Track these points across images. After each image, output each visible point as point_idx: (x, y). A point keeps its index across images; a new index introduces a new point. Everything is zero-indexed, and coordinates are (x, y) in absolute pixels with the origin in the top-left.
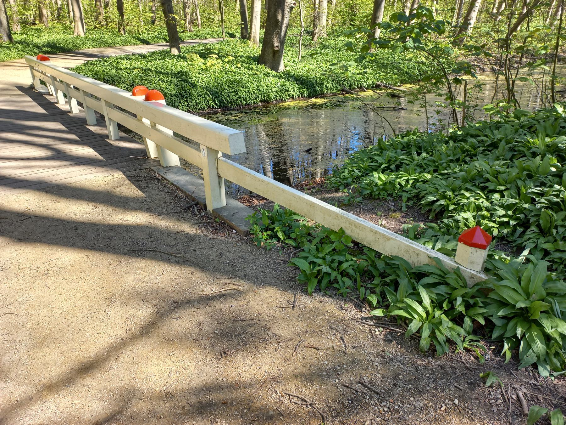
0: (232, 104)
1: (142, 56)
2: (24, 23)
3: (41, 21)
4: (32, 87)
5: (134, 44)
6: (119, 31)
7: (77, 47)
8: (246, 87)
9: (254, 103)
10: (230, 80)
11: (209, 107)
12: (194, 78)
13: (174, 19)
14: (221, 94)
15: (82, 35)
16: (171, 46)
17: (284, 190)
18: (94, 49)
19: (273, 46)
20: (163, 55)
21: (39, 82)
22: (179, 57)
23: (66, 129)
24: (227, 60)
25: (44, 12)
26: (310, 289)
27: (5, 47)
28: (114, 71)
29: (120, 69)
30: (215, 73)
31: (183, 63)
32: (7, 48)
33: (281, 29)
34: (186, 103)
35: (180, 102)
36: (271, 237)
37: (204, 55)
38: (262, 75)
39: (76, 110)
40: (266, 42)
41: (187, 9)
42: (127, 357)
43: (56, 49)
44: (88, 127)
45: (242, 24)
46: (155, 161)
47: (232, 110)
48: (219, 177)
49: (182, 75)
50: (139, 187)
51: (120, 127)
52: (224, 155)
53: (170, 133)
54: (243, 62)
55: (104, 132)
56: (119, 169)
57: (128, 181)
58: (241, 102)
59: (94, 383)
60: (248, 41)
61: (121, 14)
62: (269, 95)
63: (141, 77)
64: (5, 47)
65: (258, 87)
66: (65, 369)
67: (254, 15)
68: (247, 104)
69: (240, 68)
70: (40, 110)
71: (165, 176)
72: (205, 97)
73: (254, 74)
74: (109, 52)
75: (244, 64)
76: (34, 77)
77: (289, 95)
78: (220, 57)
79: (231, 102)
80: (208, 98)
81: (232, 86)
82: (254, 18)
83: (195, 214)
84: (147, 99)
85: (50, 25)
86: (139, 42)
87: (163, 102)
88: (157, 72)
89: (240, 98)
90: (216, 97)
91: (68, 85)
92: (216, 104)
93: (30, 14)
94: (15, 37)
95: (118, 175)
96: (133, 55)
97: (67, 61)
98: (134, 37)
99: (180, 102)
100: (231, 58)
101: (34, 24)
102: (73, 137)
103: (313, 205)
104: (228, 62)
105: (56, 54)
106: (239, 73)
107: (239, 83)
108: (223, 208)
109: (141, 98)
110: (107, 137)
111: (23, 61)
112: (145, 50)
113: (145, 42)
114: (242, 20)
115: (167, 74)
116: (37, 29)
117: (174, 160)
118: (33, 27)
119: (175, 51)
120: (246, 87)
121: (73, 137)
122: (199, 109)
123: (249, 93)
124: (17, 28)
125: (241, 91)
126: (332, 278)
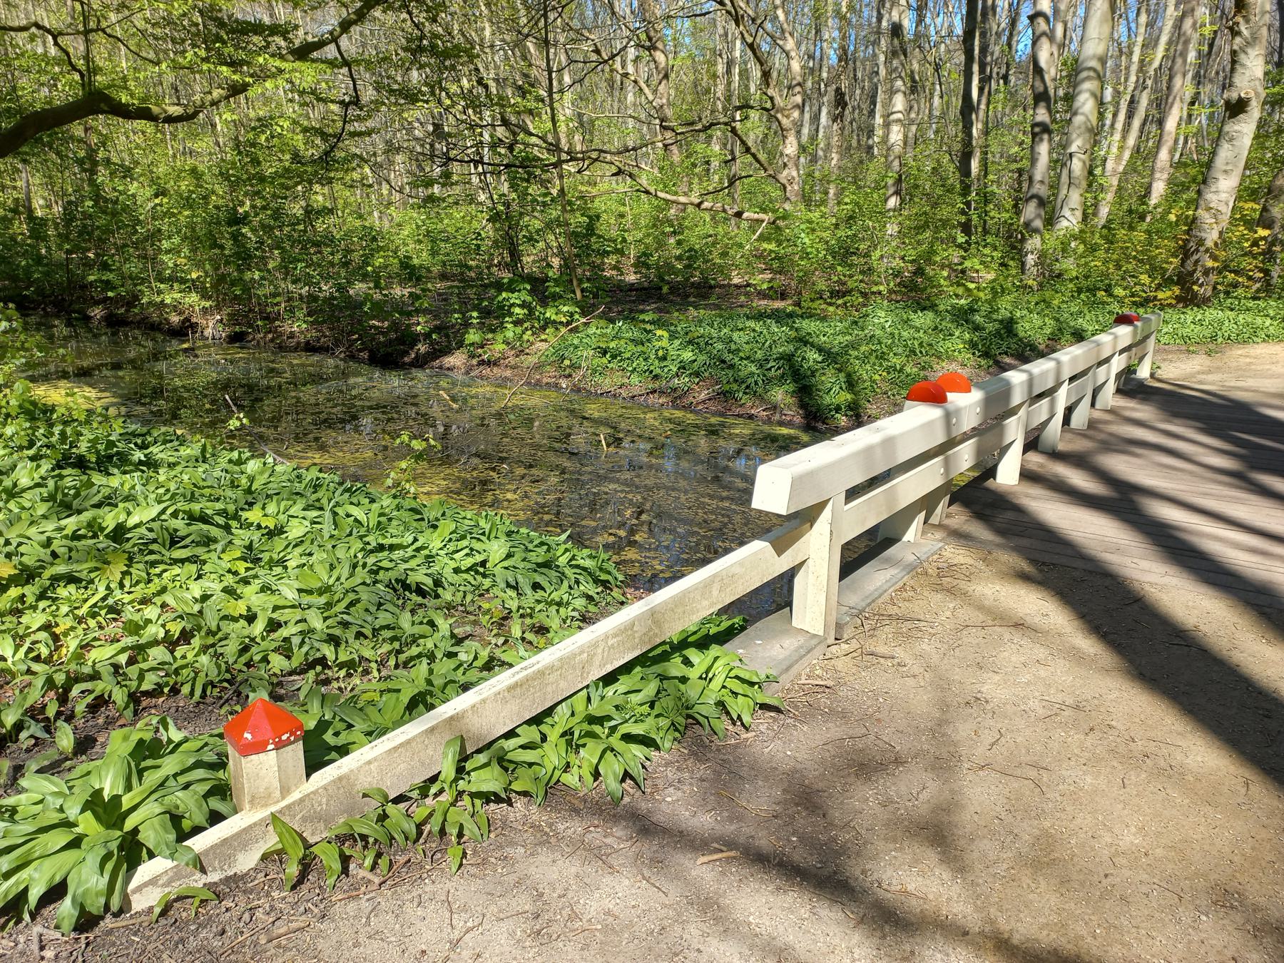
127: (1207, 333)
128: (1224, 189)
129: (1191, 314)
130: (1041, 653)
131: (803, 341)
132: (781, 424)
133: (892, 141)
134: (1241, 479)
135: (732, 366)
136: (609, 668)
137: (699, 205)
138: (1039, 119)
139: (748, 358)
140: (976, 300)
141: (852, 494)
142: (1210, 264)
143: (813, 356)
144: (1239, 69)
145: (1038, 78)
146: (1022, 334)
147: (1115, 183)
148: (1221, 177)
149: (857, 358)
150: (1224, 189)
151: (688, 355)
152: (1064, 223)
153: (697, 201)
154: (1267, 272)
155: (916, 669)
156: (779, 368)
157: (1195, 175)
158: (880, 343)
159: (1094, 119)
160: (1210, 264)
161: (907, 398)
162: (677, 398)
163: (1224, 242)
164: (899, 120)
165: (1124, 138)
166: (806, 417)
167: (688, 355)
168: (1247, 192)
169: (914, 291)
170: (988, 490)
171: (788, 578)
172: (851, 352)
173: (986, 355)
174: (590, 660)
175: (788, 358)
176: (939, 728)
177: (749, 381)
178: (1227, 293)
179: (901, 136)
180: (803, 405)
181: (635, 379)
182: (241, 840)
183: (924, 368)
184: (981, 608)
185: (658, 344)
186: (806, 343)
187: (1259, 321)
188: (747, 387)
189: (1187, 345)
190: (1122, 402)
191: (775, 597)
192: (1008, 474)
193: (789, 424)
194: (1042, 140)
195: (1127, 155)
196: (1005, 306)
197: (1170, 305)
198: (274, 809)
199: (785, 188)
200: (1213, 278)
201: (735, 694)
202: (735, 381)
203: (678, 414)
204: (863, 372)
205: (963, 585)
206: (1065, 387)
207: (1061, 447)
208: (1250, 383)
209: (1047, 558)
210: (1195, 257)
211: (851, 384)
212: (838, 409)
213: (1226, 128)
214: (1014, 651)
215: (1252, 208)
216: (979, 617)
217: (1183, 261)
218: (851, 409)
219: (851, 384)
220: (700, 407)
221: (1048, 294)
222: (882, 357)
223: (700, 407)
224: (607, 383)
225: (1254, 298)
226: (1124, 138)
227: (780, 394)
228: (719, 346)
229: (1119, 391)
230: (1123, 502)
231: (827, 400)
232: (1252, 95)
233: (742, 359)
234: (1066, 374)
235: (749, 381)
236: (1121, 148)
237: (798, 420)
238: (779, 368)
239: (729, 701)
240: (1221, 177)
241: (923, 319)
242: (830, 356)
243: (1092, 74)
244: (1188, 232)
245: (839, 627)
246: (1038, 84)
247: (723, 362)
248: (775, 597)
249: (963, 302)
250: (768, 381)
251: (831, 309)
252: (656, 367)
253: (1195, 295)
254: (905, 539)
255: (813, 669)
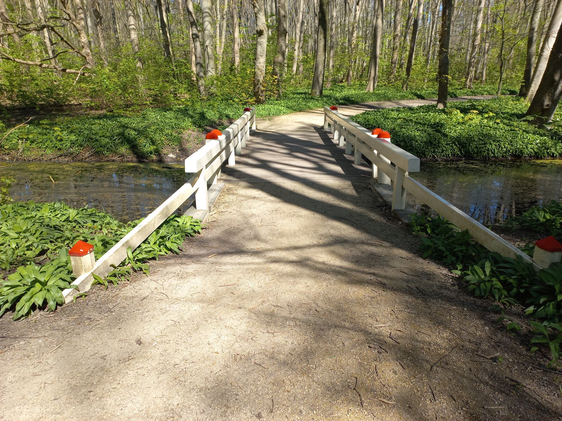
0: (478, 155)
1: (411, 109)
2: (335, 81)
3: (347, 80)
4: (322, 128)
5: (410, 99)
6: (402, 88)
7: (363, 100)
8: (498, 141)
9: (503, 156)
10: (483, 134)
11: (454, 155)
12: (448, 130)
13: (447, 79)
14: (469, 145)
15: (371, 91)
16: (439, 101)
17: (437, 200)
18: (376, 102)
19: (542, 105)
20: (428, 109)
21: (327, 125)
22: (443, 111)
23: (343, 172)
24: (486, 115)
25: (351, 73)
26: (425, 255)
27: (316, 99)
28: (382, 120)
29: (388, 118)
30: (470, 126)
31: (444, 116)
32: (317, 100)
33: (555, 90)
34: (432, 150)
35: (428, 148)
36: (422, 230)
37: (465, 111)
38: (521, 131)
39: (342, 143)
40: (537, 101)
41: (471, 68)
42: (313, 250)
43: (348, 102)
44: (354, 165)
45: (523, 82)
46: (375, 179)
47: (476, 160)
48: (403, 188)
49: (438, 126)
50: (357, 192)
51: (363, 157)
52: (410, 174)
53: (389, 162)
54: (504, 118)
55: (352, 158)
56: (351, 180)
57: (352, 187)
58: (488, 154)
59: (298, 252)
60: (522, 99)
61: (408, 74)
62: (521, 151)
63: (402, 125)
64: (316, 99)
65: (511, 142)
66: (288, 246)
67: (537, 74)
68: (494, 157)
69: (498, 124)
70: (321, 142)
71: (376, 188)
72: (452, 146)
73: (511, 130)
74: (388, 105)
75: (505, 121)
76: (325, 120)
77: (548, 153)
78: (481, 113)
79: (477, 153)
80: (455, 147)
81: (482, 139)
82: (536, 76)
83: (382, 211)
84: (379, 137)
85: (352, 83)
86: (415, 97)
87: (389, 140)
88: (416, 122)
89: (488, 150)
90: (463, 147)
91: (342, 127)
92: (461, 153)
93: (340, 75)
94: (325, 92)
95: (348, 183)
96: (404, 107)
97: (352, 110)
98: (412, 93)
99: (428, 148)
100: (491, 114)
101: (341, 82)
102: (333, 160)
103: (453, 211)
104: (487, 118)
105: (347, 105)
106: (496, 128)
107: (492, 136)
108: (401, 210)
109: (375, 136)
110: (353, 162)
111: (323, 109)
112: (416, 104)
113: (421, 97)
114: (524, 78)
115: (425, 124)
116: (342, 86)
117: (387, 180)
118: (340, 84)
119: (441, 106)
120: (498, 141)
121: (333, 160)
122: (444, 156)
123: (500, 146)
124: (329, 85)
125: (491, 144)
126: (444, 255)
127: (267, 113)
128: (262, 61)
129: (261, 107)
130: (263, 202)
131: (125, 127)
132: (128, 162)
133: (133, 38)
134: (290, 155)
135: (97, 140)
136: (160, 224)
137: (41, 65)
138: (194, 32)
139: (103, 136)
140: (187, 106)
141: (207, 166)
142: (263, 89)
143: (133, 132)
144: (259, 20)
145: (190, 16)
146: (209, 118)
147: (221, 56)
148: (260, 58)
149: (152, 132)
150: (262, 61)
151: (73, 137)
152: (210, 74)
153: (39, 63)
154: (278, 91)
155: (235, 212)
156: (119, 139)
157: (250, 56)
158: (159, 125)
159: (212, 32)
160: (263, 89)
161: (206, 138)
162: (74, 157)
163: (265, 81)
164: (133, 29)
165: (220, 39)
166: (137, 158)
167: (73, 137)
168: (269, 62)
169: (160, 103)
170: (228, 168)
171: (193, 196)
172: (148, 130)
173: (200, 126)
174: (155, 222)
175: (122, 134)
176: (247, 223)
177: (108, 146)
178: (269, 99)
179: (136, 36)
180: (135, 153)
181: (48, 151)
182: (84, 283)
183: (179, 133)
184: (243, 196)
185: (56, 134)
186: (127, 128)
187: (280, 108)
188: (107, 148)
189: (263, 118)
190: (252, 138)
191: (191, 202)
192: (232, 163)
193: (132, 161)
194: (197, 41)
195: (223, 45)
196: (198, 107)
197: (254, 104)
198: (92, 271)
199: (85, 58)
200: (264, 93)
201: (195, 226)
202: (101, 146)
203: (79, 164)
204: (157, 137)
205: (235, 192)
206: (240, 132)
207: (242, 153)
208: (283, 128)
209: (254, 182)
210: (258, 86)
211: (153, 142)
212: (151, 153)
213: (258, 40)
214: (256, 203)
215: (270, 68)
216: (244, 198)
217: (254, 88)
218: (156, 152)
219: (153, 142)
220: (87, 160)
221: (212, 102)
222: (161, 130)
223: (87, 160)
224: (33, 155)
225: (277, 100)
226: (220, 39)
227: (124, 149)
228: (87, 132)
229: (250, 135)
230: (264, 165)
231: (145, 150)
232: (264, 29)
233: (100, 137)
234: (240, 130)
235: (108, 146)
236: (221, 42)
237: (134, 159)
238: (119, 139)
239: (194, 227)
240: (260, 58)
241: (169, 114)
242: (140, 132)
243: (207, 14)
244: (254, 77)
245: (210, 207)
246: (191, 18)
247: (92, 139)
248: (191, 202)
249: (181, 106)
250: (116, 145)
251: (128, 112)
252: (59, 145)
253: (260, 100)
254: (213, 184)
255: (207, 218)
